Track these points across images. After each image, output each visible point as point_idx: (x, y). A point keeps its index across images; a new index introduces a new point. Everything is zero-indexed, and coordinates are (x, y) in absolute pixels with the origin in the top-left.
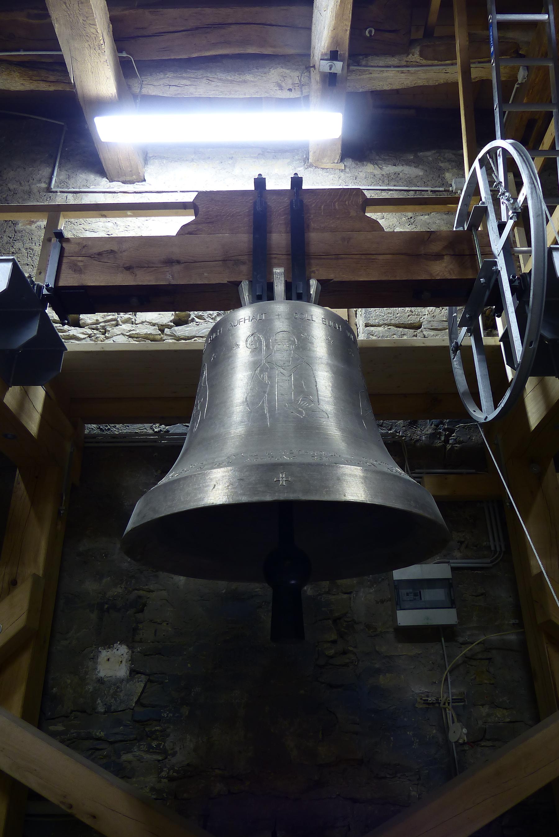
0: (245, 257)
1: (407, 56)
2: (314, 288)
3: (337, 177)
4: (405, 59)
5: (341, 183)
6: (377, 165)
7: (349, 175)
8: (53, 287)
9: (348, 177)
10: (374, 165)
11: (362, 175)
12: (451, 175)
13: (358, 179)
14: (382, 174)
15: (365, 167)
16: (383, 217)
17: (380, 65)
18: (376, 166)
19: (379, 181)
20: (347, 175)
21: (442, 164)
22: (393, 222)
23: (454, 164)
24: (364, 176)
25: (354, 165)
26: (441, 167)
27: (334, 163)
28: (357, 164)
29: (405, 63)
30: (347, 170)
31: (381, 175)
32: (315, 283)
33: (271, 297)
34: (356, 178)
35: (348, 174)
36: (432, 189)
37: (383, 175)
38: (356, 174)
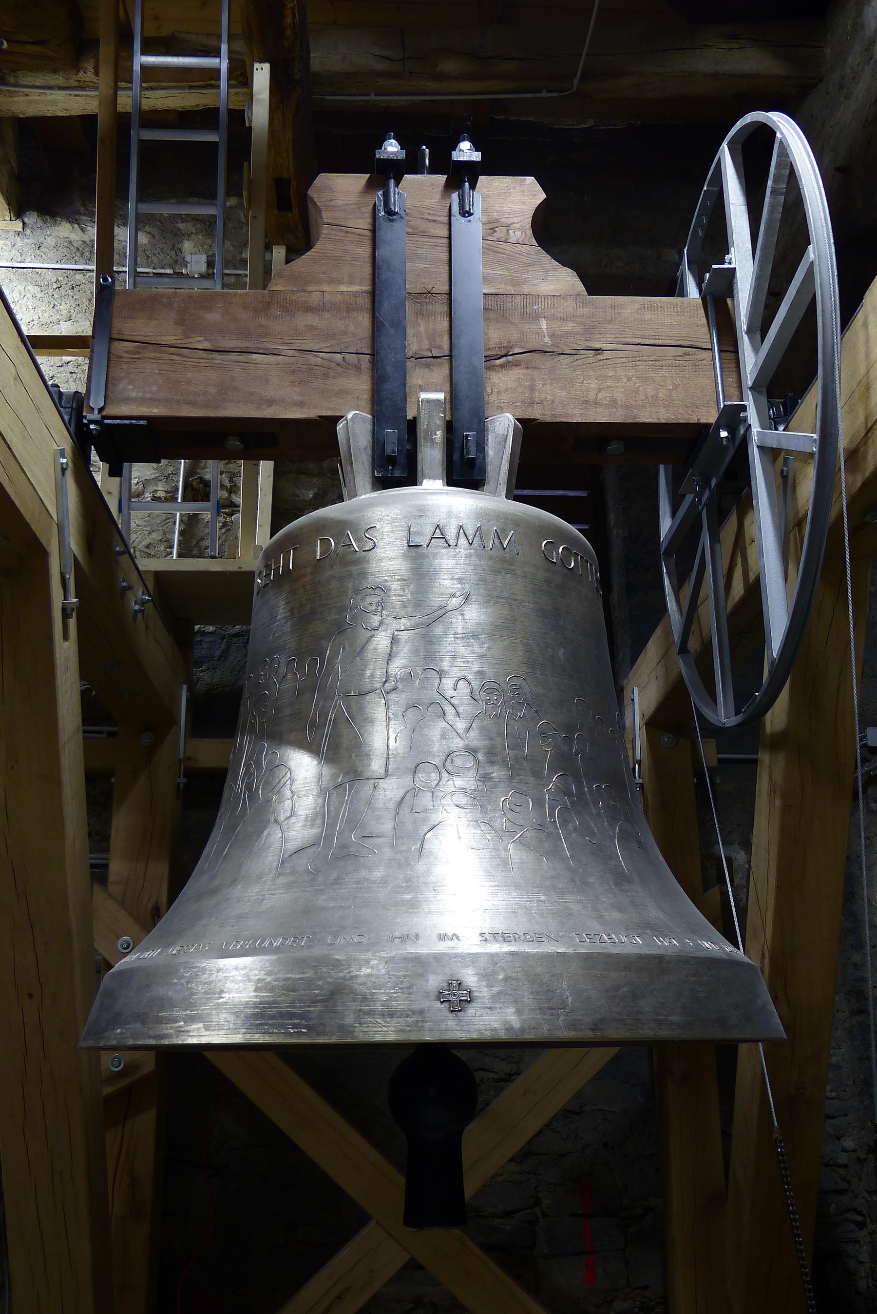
0: (360, 301)
1: (77, 74)
2: (420, 434)
3: (9, 244)
4: (75, 78)
5: (15, 255)
6: (78, 224)
7: (30, 241)
8: (368, 175)
9: (27, 244)
10: (72, 223)
11: (50, 241)
12: (193, 245)
13: (42, 248)
14: (83, 239)
15: (56, 227)
16: (70, 317)
17: (37, 84)
18: (76, 226)
19: (76, 253)
20: (27, 240)
21: (182, 224)
22: (84, 328)
23: (199, 225)
24: (53, 244)
25: (40, 223)
26: (179, 230)
27: (5, 220)
28: (45, 222)
29: (76, 84)
30: (28, 232)
31: (80, 243)
32: (341, 423)
33: (411, 478)
34: (40, 246)
35: (28, 239)
36: (154, 271)
37: (84, 242)
38: (42, 239)
